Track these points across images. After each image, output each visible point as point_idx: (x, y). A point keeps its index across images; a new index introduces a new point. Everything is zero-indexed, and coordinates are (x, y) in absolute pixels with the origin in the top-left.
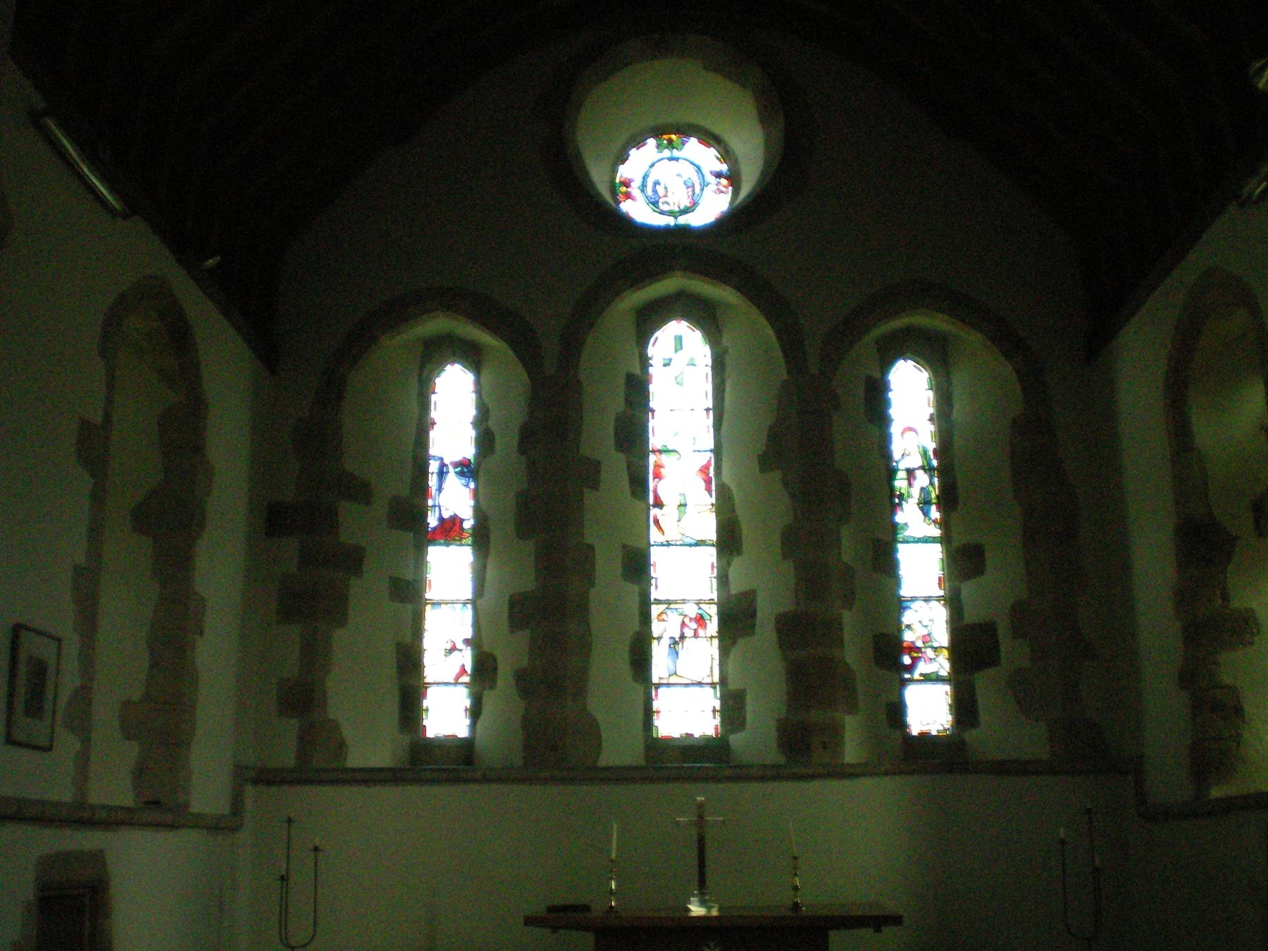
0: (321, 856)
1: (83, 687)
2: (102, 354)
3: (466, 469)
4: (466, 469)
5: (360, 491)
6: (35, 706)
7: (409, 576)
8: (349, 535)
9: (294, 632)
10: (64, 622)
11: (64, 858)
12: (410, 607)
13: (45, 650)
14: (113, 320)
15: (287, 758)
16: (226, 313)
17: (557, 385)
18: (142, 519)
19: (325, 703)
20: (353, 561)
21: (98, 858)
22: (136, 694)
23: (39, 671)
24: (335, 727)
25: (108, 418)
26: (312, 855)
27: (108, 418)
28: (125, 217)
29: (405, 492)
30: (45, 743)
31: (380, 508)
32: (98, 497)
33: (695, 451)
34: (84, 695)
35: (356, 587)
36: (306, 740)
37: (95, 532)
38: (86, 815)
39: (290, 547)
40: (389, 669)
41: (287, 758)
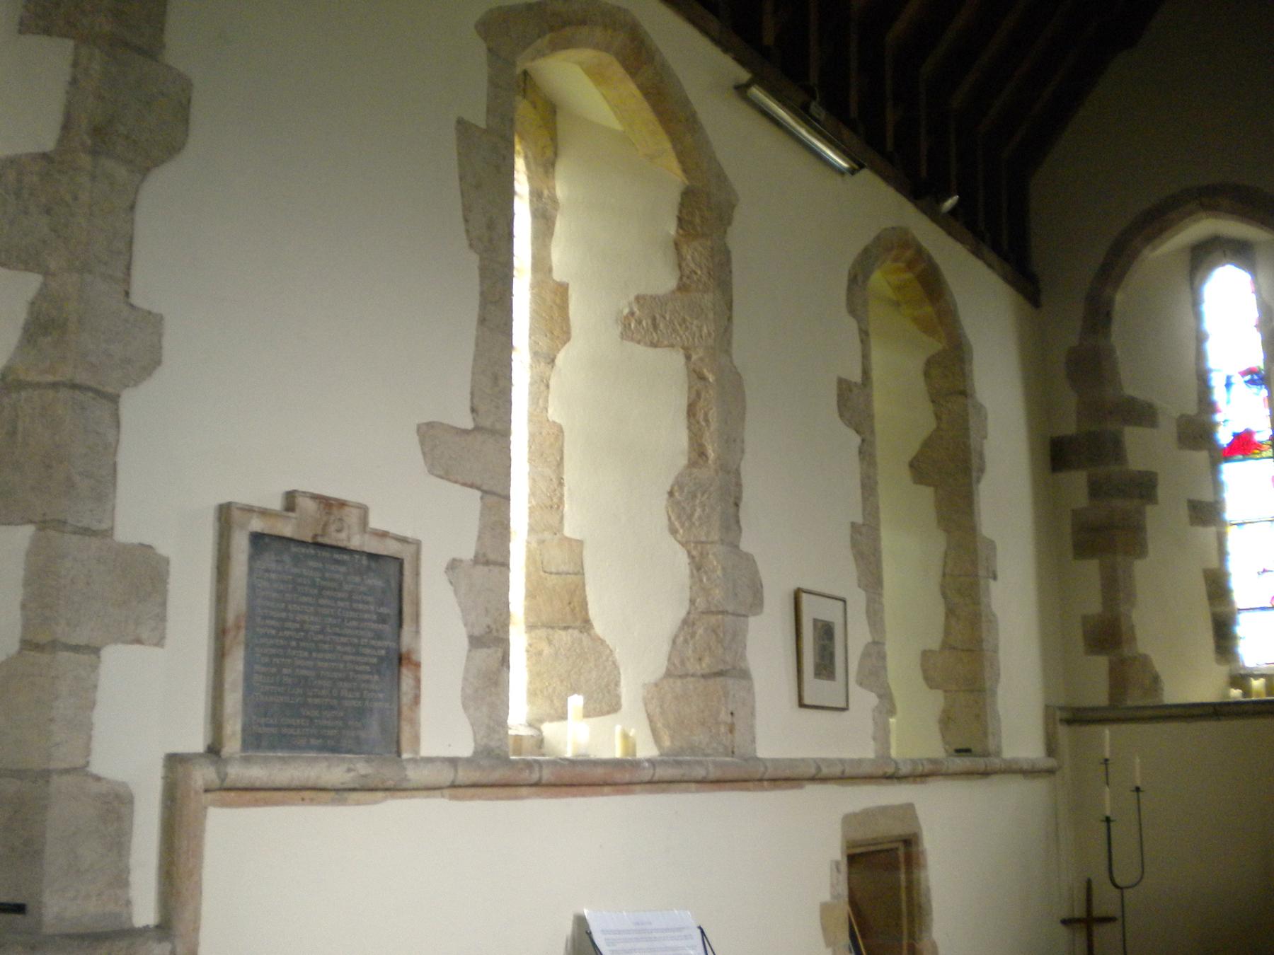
0: (1141, 794)
1: (875, 643)
2: (852, 311)
3: (1255, 378)
4: (1255, 378)
5: (1143, 414)
6: (825, 667)
7: (1207, 497)
8: (1136, 460)
9: (1091, 568)
10: (844, 581)
11: (868, 815)
12: (1212, 530)
13: (830, 612)
14: (857, 279)
15: (1098, 695)
16: (977, 253)
17: (16, 812)
18: (921, 469)
19: (1133, 639)
20: (1144, 487)
21: (909, 809)
22: (934, 643)
23: (826, 632)
24: (1145, 661)
25: (866, 373)
26: (1135, 793)
27: (866, 373)
28: (852, 172)
29: (1192, 409)
30: (842, 705)
31: (1166, 431)
32: (866, 453)
33: (700, 928)
34: (876, 651)
35: (1152, 514)
36: (1119, 679)
37: (869, 487)
38: (890, 770)
39: (1076, 482)
40: (1201, 589)
41: (1098, 695)
